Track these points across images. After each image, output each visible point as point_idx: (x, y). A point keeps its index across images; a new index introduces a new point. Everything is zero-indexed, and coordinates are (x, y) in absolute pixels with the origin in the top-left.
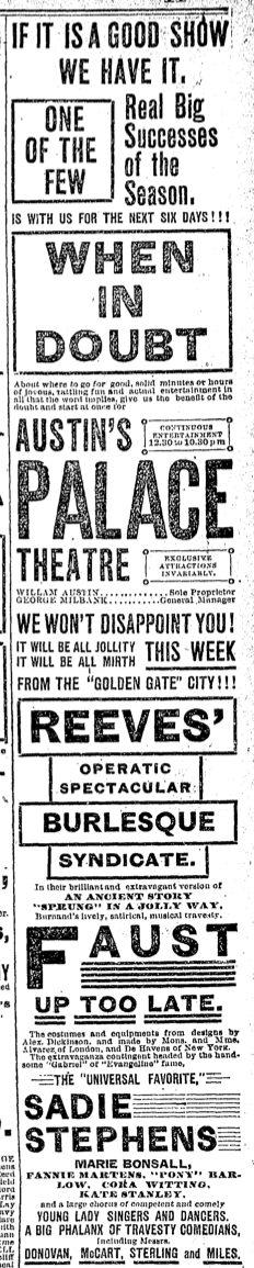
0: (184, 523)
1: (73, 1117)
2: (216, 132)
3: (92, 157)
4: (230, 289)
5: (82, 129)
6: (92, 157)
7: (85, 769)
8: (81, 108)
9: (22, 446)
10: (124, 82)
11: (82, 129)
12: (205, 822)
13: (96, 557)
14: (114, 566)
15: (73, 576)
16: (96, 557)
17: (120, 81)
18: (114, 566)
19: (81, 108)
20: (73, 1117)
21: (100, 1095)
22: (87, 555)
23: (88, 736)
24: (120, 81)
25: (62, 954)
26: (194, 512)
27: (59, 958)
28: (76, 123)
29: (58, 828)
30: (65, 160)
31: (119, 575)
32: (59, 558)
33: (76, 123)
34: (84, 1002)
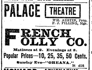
0: (31, 14)
1: (17, 16)
2: (85, 56)
3: (74, 13)
4: (89, 12)
5: (75, 14)
6: (74, 13)
7: (50, 63)
8: (75, 8)
9: (13, 15)
10: (64, 14)
11: (75, 14)
12: (72, 11)
13: (68, 9)
14: (72, 11)
15: (25, 15)
16: (68, 9)
17: (63, 14)
18: (72, 11)
19: (75, 8)
20: (17, 16)
21: (11, 16)
22: (66, 9)
23: (21, 15)
24: (63, 14)
25: (15, 36)
26: (33, 12)
27: (14, 37)
28: (58, 12)
29: (74, 66)
30: (51, 14)
31: (36, 14)
32: (60, 9)
33: (58, 12)
34: (50, 8)
